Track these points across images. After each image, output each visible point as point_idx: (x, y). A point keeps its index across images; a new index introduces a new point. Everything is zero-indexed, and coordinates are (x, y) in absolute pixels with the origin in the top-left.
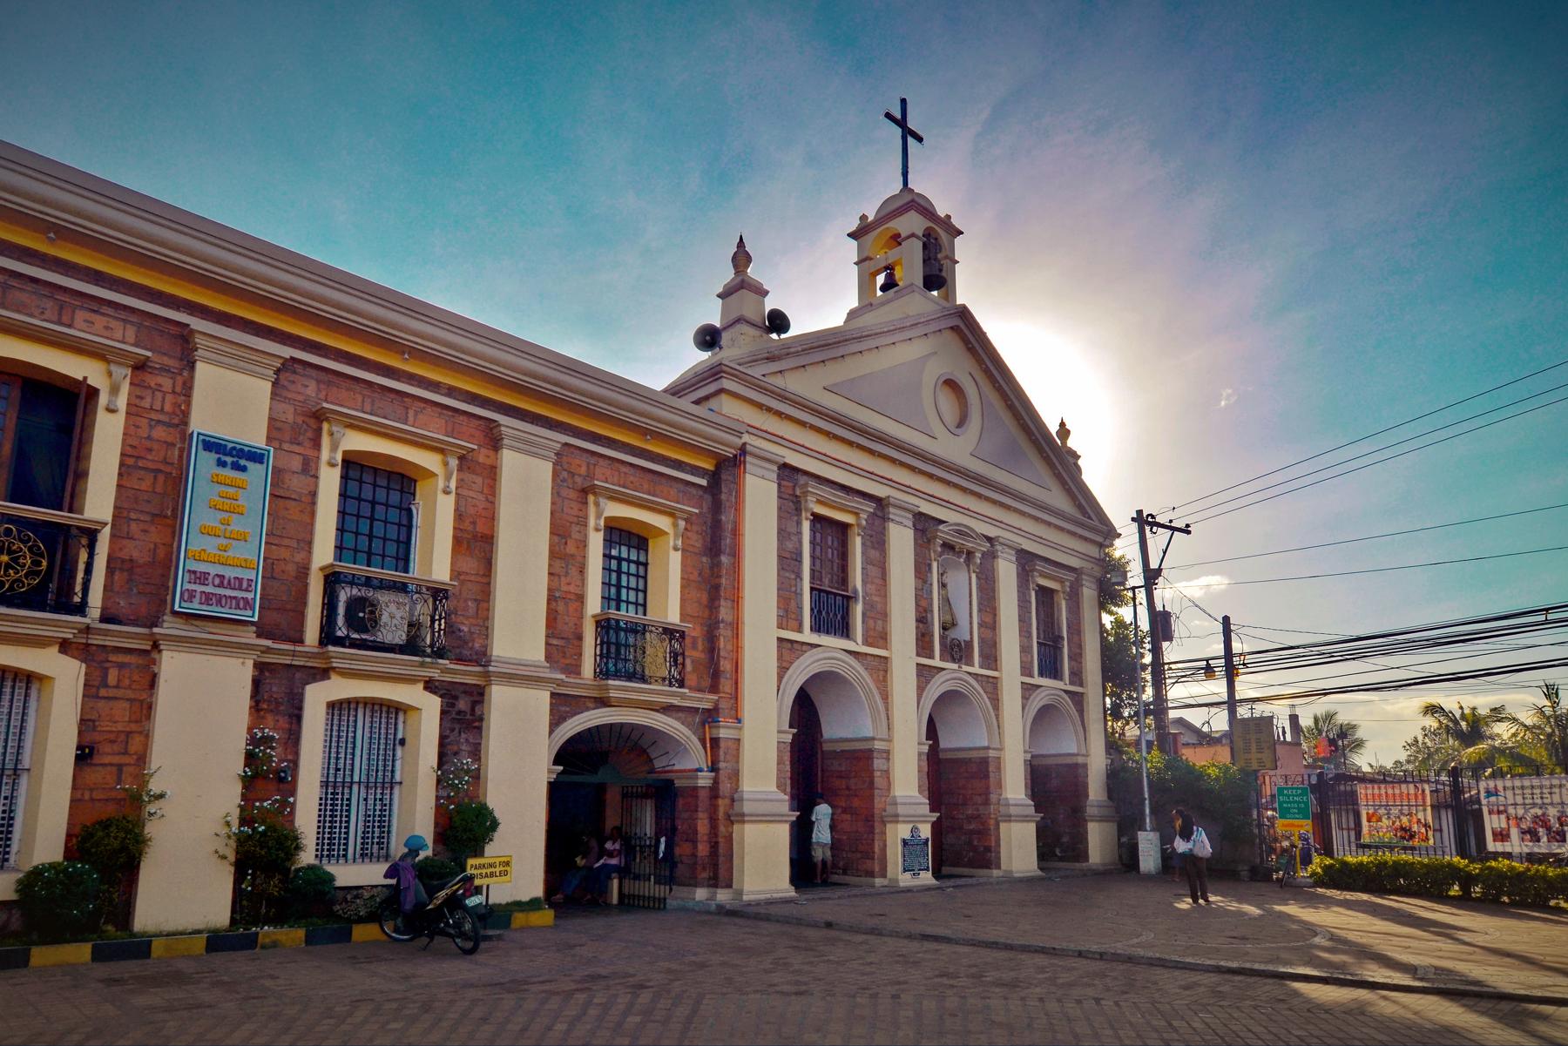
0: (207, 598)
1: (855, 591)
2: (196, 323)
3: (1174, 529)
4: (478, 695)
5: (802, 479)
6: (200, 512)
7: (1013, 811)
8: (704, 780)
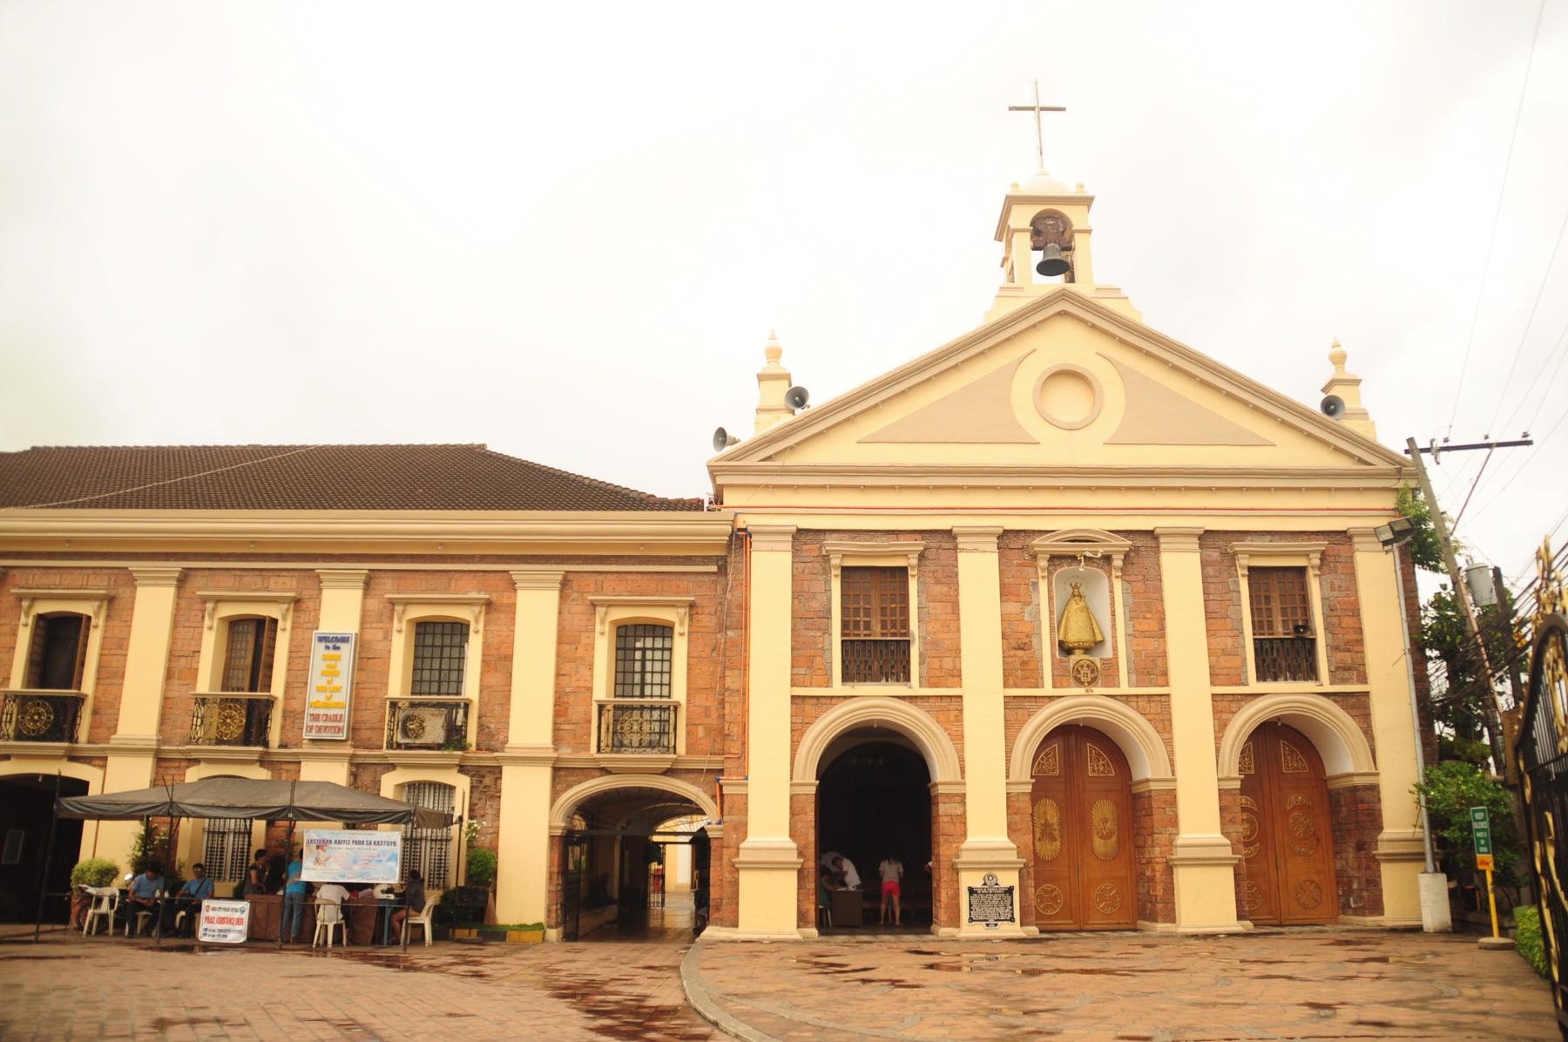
0: (319, 729)
2: (132, 565)
3: (1489, 446)
4: (497, 772)
6: (316, 679)
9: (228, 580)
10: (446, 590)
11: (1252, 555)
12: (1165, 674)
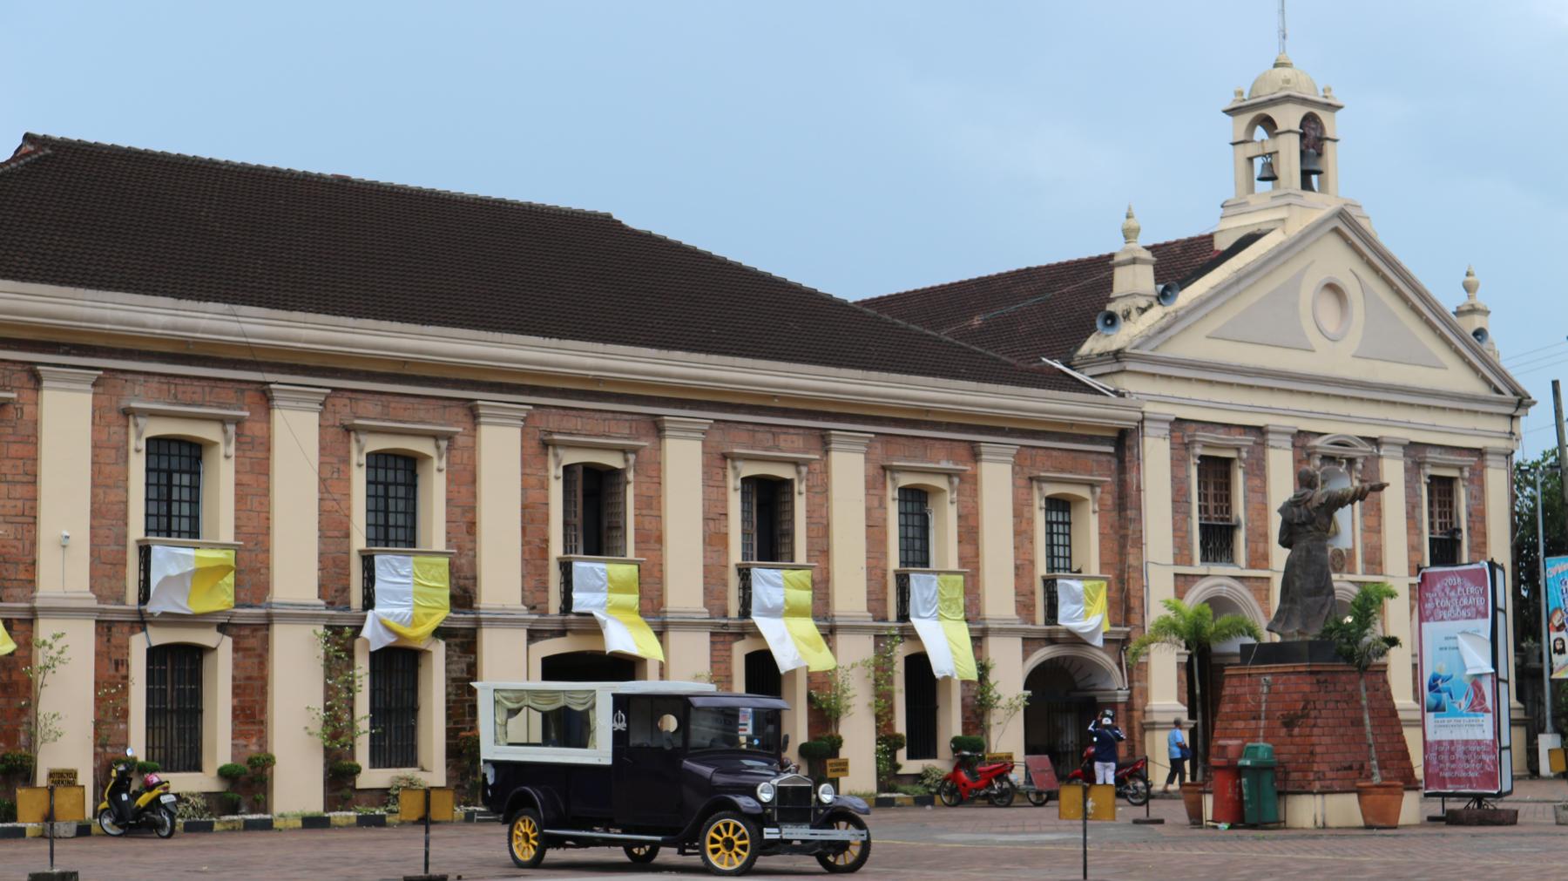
1: (1238, 521)
5: (1191, 429)
7: (1157, 718)
8: (1122, 697)
9: (766, 437)
10: (924, 459)
11: (1434, 465)
12: (1380, 564)
